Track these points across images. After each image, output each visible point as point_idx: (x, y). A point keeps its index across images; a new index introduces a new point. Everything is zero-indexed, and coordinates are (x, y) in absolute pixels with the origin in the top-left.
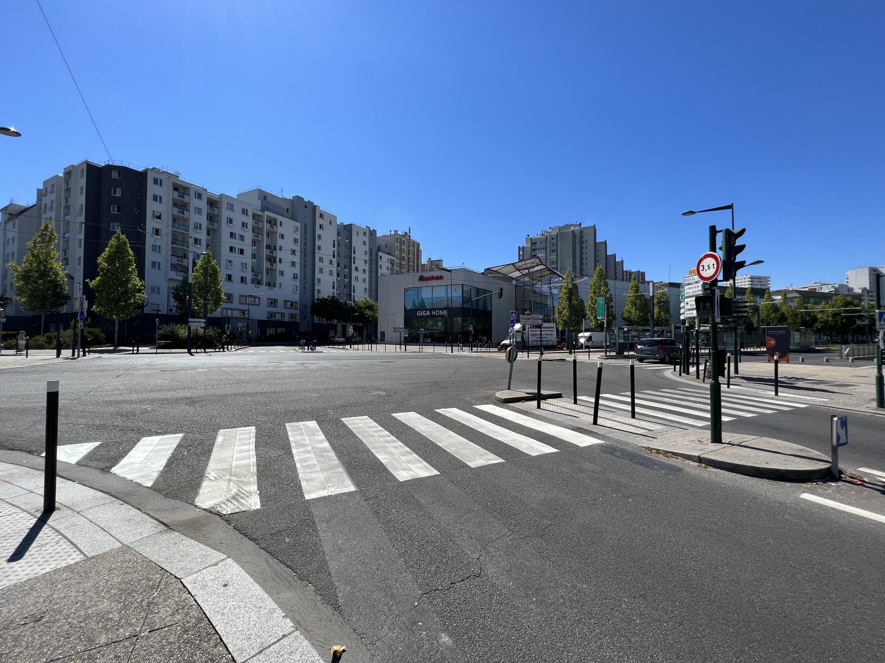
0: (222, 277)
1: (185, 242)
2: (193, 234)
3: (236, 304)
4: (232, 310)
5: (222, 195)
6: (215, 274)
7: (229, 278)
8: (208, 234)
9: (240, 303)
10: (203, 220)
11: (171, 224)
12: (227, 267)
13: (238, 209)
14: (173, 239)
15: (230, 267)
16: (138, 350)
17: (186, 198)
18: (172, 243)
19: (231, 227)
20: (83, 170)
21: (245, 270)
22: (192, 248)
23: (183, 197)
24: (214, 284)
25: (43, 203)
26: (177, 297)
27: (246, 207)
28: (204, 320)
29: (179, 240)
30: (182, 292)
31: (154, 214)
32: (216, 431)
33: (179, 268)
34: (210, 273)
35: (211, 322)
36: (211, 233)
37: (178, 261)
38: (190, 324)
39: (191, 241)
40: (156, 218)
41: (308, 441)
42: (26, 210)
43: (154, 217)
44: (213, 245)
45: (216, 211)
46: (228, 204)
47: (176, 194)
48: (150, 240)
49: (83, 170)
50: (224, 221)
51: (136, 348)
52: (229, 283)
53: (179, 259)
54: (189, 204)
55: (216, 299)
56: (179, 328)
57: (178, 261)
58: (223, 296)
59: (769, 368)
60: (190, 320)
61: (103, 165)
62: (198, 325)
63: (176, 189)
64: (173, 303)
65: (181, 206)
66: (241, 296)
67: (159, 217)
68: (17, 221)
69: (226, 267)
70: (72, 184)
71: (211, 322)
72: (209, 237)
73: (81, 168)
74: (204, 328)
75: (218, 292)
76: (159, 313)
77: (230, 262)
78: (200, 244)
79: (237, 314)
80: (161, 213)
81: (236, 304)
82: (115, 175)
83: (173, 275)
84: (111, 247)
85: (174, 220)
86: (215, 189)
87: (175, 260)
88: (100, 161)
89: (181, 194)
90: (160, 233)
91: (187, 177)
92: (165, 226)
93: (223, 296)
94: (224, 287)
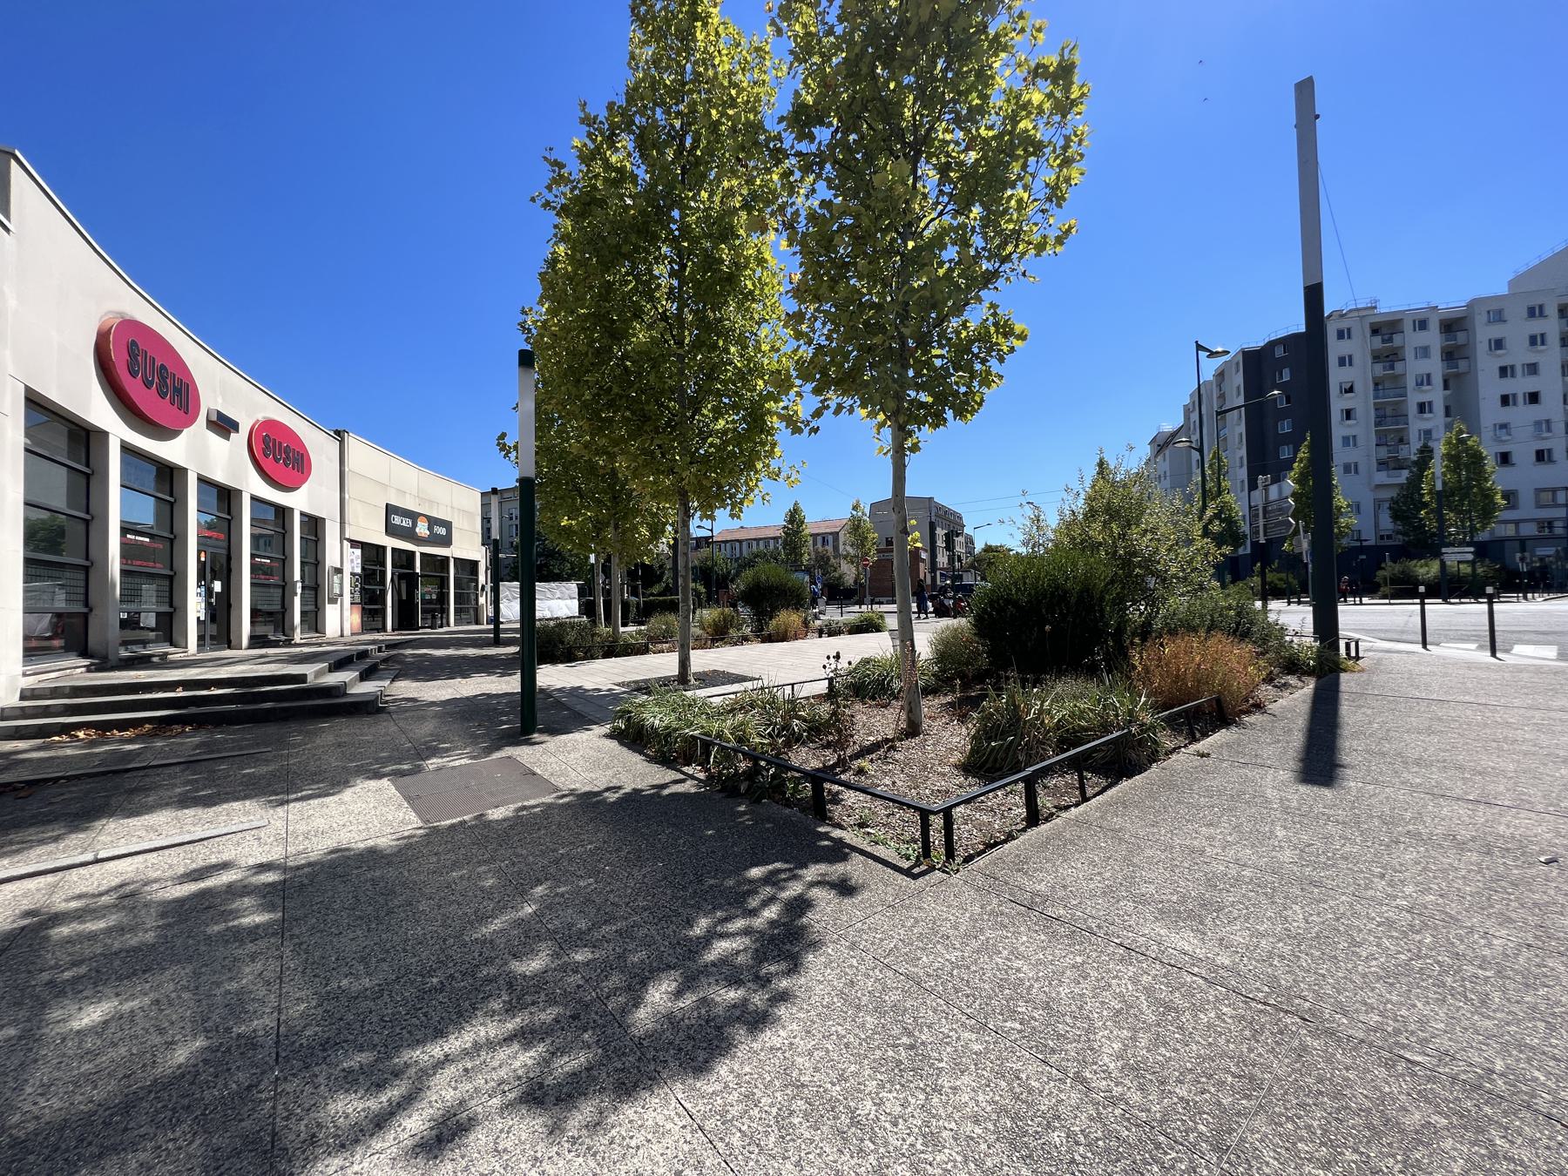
0: (1490, 463)
1: (1401, 416)
2: (1414, 398)
3: (1527, 509)
4: (1517, 523)
5: (1471, 305)
6: (1477, 459)
7: (1505, 459)
8: (1446, 387)
9: (1539, 506)
10: (1435, 366)
11: (1372, 392)
12: (1498, 440)
13: (1517, 312)
14: (1377, 417)
15: (1504, 438)
16: (1361, 601)
17: (1397, 340)
18: (1376, 425)
19: (1499, 356)
20: (1238, 364)
21: (1546, 435)
22: (1416, 425)
23: (1390, 340)
24: (1477, 481)
25: (1192, 421)
26: (1396, 516)
27: (1535, 302)
28: (1472, 549)
29: (1389, 420)
30: (1405, 506)
31: (1341, 387)
32: (614, 803)
33: (1392, 465)
34: (1467, 461)
35: (1482, 550)
36: (1451, 383)
37: (1389, 452)
38: (1446, 557)
39: (1412, 409)
40: (1346, 392)
41: (1259, 1073)
42: (1174, 434)
43: (1341, 392)
44: (1460, 407)
45: (1461, 337)
46: (1489, 312)
47: (1377, 341)
48: (1339, 430)
49: (1238, 364)
50: (1482, 348)
51: (1357, 599)
52: (1506, 470)
53: (1391, 448)
54: (1403, 347)
55: (1483, 509)
56: (1415, 566)
57: (1389, 452)
58: (1499, 501)
59: (554, 603)
60: (1444, 550)
61: (1262, 344)
62: (1458, 558)
63: (1375, 331)
64: (1387, 523)
65: (1387, 356)
66: (1538, 491)
67: (1351, 390)
68: (1167, 452)
69: (1495, 440)
70: (1226, 387)
71: (1482, 550)
72: (1448, 392)
73: (1236, 360)
74: (1472, 563)
75: (1488, 495)
76: (1364, 544)
77: (1504, 426)
78: (1431, 411)
79: (1529, 530)
80: (1352, 382)
81: (1527, 509)
82: (1279, 352)
83: (1382, 477)
84: (1301, 461)
85: (1376, 384)
86: (1451, 297)
87: (1383, 453)
88: (1257, 341)
89: (1386, 337)
90: (1352, 415)
91: (1390, 304)
92: (1363, 402)
93: (1498, 499)
94: (1498, 480)
